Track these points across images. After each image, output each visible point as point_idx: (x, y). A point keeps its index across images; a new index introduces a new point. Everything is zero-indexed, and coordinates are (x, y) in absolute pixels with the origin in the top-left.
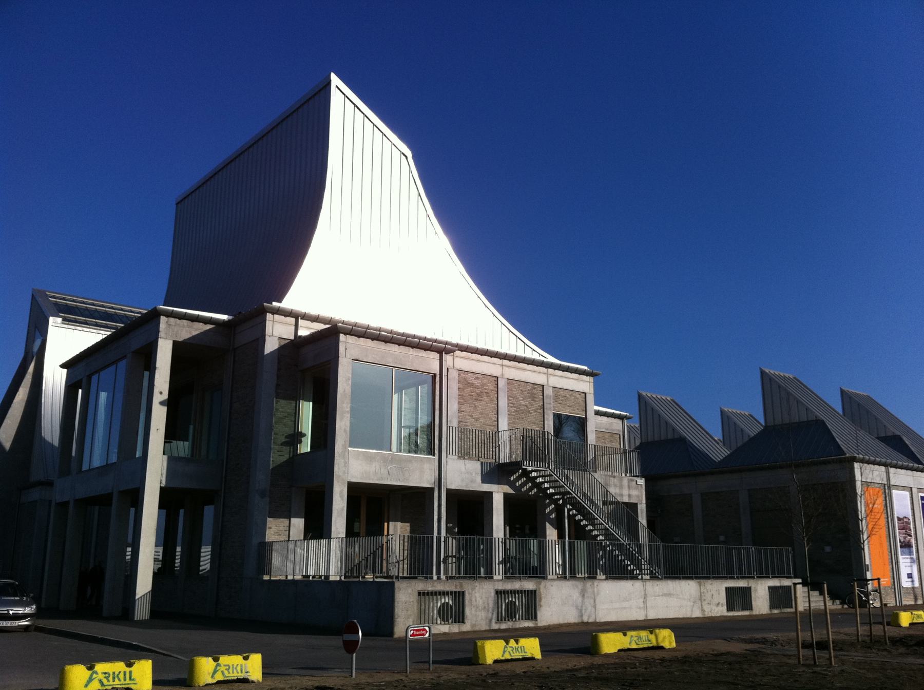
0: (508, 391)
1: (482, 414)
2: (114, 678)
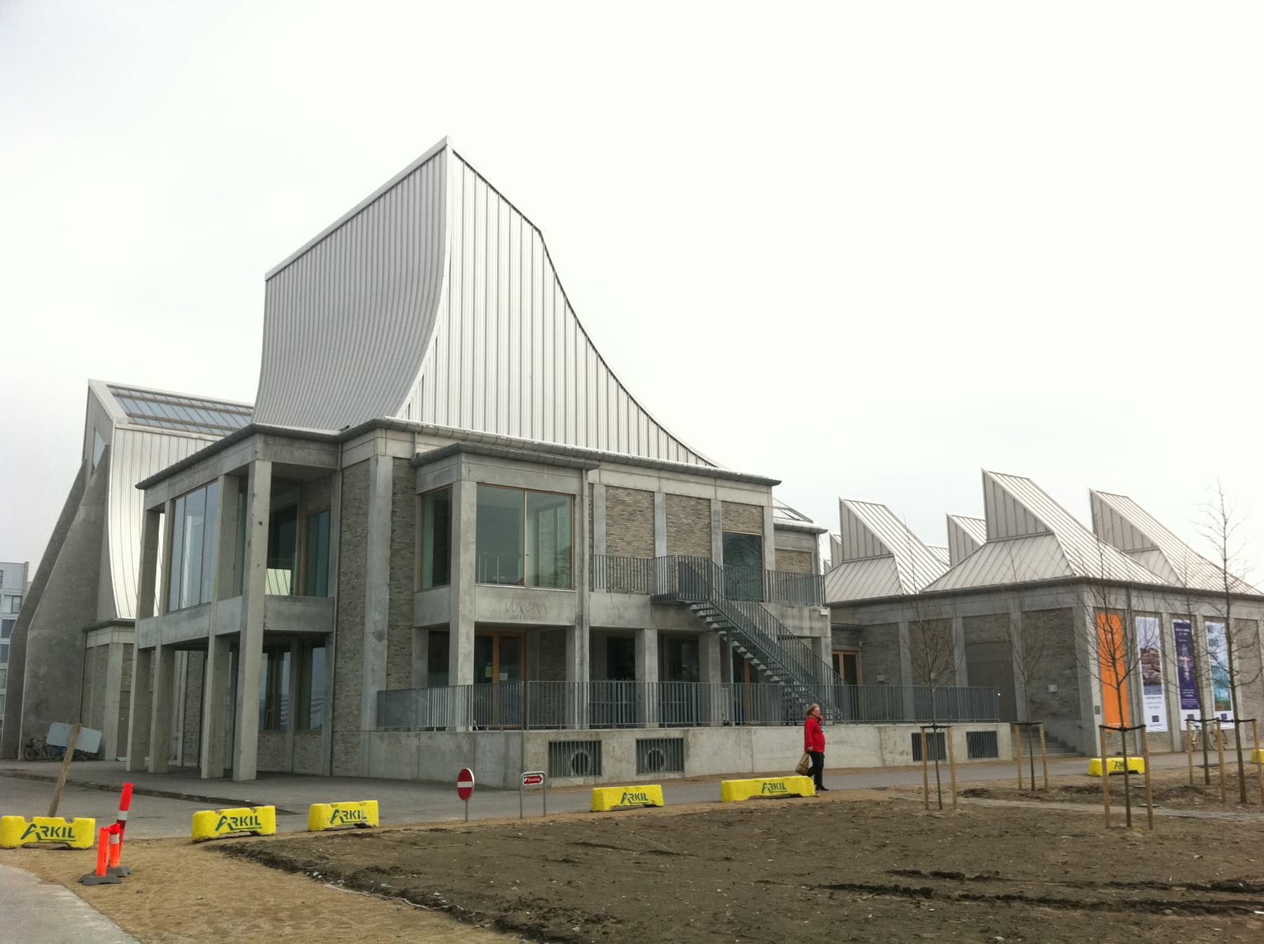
1: (635, 536)
2: (241, 822)
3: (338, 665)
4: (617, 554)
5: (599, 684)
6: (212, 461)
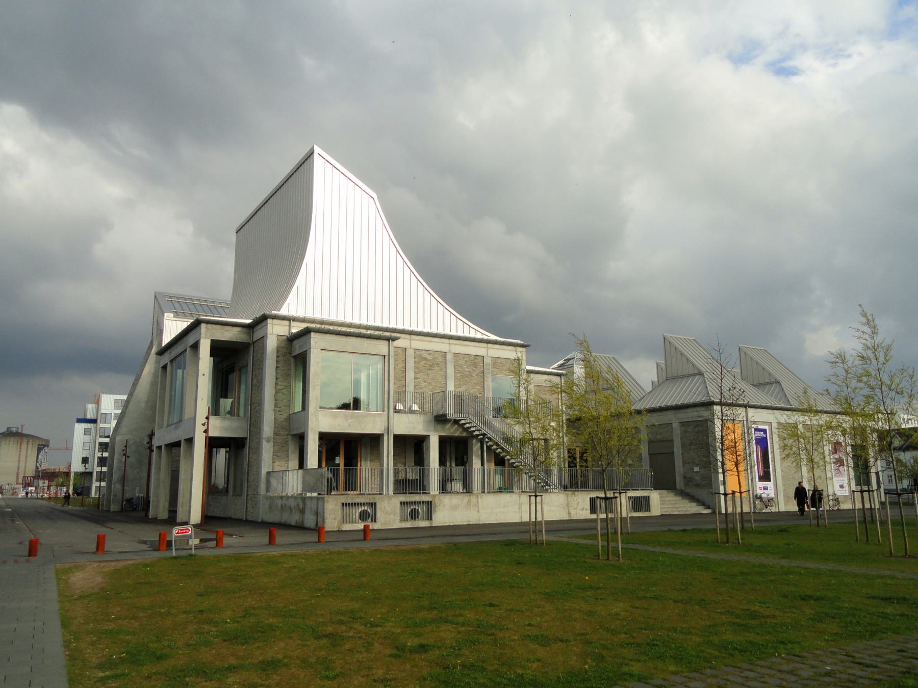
0: (454, 362)
3: (250, 457)
4: (421, 391)
5: (352, 469)
6: (185, 339)
